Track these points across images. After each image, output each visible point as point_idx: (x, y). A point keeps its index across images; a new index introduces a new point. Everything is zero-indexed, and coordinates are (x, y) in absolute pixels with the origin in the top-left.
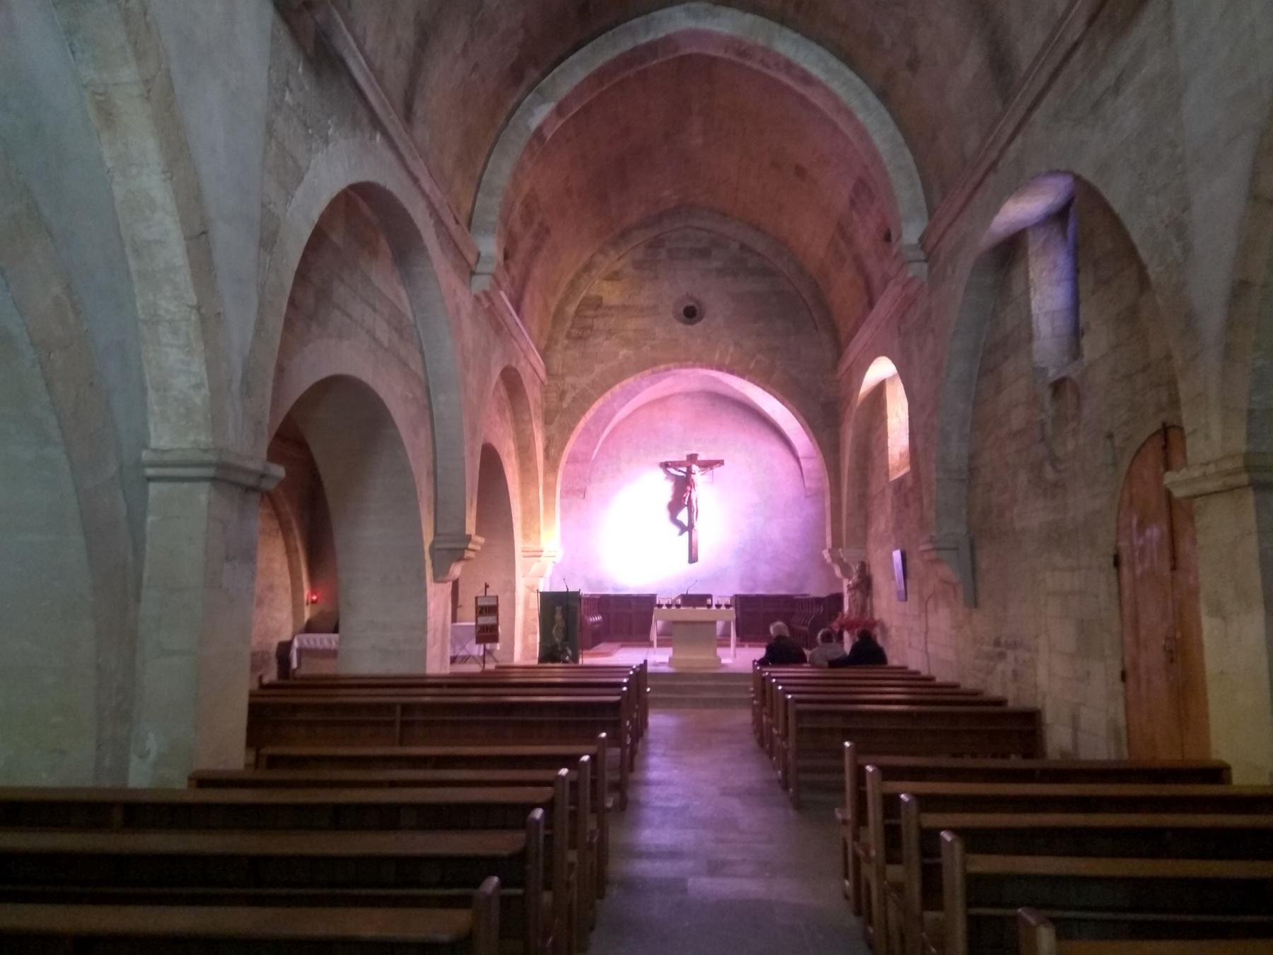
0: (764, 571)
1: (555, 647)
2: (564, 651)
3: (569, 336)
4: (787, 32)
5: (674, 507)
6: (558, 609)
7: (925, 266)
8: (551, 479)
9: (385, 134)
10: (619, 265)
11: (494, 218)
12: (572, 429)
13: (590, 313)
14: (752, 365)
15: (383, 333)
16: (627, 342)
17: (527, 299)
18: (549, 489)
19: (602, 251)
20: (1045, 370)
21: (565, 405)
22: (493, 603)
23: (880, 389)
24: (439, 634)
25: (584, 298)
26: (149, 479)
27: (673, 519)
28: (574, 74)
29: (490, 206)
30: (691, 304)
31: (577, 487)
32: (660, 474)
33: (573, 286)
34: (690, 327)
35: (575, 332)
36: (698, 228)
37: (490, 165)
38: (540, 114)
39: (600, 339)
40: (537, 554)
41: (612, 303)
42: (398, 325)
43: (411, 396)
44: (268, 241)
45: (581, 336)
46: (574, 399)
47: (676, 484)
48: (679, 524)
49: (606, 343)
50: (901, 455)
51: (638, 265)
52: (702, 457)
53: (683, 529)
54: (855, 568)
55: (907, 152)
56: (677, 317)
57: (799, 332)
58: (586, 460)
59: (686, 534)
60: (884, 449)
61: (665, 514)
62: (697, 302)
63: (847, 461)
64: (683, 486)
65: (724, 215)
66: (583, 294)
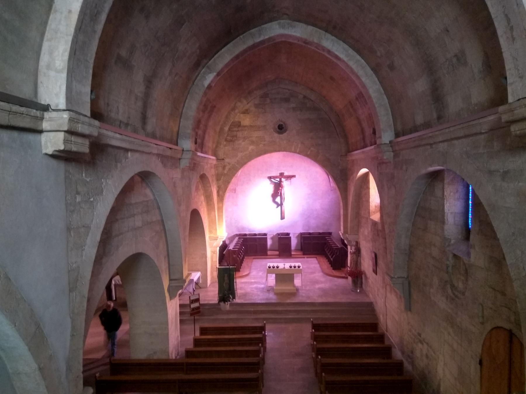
4: (329, 36)
6: (226, 275)
8: (221, 205)
9: (131, 150)
11: (189, 131)
14: (309, 153)
16: (252, 143)
20: (451, 240)
21: (225, 172)
22: (197, 297)
23: (366, 175)
24: (174, 320)
25: (233, 122)
28: (225, 57)
30: (282, 123)
32: (268, 182)
33: (227, 117)
34: (281, 135)
35: (229, 138)
37: (186, 105)
39: (240, 142)
41: (245, 125)
45: (232, 140)
46: (230, 169)
47: (275, 186)
49: (243, 143)
50: (376, 207)
51: (257, 106)
52: (286, 174)
54: (354, 243)
55: (385, 97)
59: (280, 207)
60: (368, 201)
61: (271, 199)
62: (284, 123)
63: (351, 198)
65: (296, 83)
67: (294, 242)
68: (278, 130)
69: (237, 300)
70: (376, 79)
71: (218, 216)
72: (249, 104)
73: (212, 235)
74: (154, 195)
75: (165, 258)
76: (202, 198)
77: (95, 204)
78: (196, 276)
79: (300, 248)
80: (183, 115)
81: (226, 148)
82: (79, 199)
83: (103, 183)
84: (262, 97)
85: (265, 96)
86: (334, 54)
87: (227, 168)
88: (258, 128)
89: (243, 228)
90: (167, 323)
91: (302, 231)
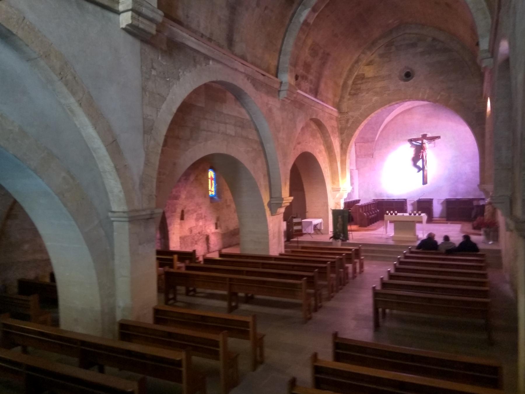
0: (461, 187)
3: (350, 94)
5: (415, 160)
6: (340, 216)
9: (213, 59)
12: (352, 136)
13: (360, 82)
14: (438, 98)
15: (231, 130)
16: (376, 94)
17: (322, 86)
18: (343, 162)
19: (363, 53)
21: (349, 125)
24: (276, 235)
25: (357, 76)
26: (113, 221)
27: (415, 165)
29: (286, 60)
30: (408, 70)
31: (369, 153)
32: (408, 145)
33: (351, 71)
34: (407, 83)
35: (353, 92)
36: (410, 34)
37: (285, 42)
38: (304, 14)
39: (364, 94)
40: (338, 190)
42: (241, 124)
44: (148, 129)
46: (353, 122)
49: (367, 95)
51: (381, 56)
52: (429, 135)
53: (420, 169)
57: (458, 76)
59: (421, 171)
61: (411, 163)
63: (488, 143)
66: (356, 74)
67: (437, 209)
68: (404, 78)
69: (350, 241)
73: (335, 186)
75: (264, 176)
76: (322, 148)
78: (316, 221)
80: (282, 52)
81: (350, 101)
82: (154, 73)
83: (180, 73)
85: (389, 45)
89: (381, 194)
90: (267, 233)
91: (448, 197)
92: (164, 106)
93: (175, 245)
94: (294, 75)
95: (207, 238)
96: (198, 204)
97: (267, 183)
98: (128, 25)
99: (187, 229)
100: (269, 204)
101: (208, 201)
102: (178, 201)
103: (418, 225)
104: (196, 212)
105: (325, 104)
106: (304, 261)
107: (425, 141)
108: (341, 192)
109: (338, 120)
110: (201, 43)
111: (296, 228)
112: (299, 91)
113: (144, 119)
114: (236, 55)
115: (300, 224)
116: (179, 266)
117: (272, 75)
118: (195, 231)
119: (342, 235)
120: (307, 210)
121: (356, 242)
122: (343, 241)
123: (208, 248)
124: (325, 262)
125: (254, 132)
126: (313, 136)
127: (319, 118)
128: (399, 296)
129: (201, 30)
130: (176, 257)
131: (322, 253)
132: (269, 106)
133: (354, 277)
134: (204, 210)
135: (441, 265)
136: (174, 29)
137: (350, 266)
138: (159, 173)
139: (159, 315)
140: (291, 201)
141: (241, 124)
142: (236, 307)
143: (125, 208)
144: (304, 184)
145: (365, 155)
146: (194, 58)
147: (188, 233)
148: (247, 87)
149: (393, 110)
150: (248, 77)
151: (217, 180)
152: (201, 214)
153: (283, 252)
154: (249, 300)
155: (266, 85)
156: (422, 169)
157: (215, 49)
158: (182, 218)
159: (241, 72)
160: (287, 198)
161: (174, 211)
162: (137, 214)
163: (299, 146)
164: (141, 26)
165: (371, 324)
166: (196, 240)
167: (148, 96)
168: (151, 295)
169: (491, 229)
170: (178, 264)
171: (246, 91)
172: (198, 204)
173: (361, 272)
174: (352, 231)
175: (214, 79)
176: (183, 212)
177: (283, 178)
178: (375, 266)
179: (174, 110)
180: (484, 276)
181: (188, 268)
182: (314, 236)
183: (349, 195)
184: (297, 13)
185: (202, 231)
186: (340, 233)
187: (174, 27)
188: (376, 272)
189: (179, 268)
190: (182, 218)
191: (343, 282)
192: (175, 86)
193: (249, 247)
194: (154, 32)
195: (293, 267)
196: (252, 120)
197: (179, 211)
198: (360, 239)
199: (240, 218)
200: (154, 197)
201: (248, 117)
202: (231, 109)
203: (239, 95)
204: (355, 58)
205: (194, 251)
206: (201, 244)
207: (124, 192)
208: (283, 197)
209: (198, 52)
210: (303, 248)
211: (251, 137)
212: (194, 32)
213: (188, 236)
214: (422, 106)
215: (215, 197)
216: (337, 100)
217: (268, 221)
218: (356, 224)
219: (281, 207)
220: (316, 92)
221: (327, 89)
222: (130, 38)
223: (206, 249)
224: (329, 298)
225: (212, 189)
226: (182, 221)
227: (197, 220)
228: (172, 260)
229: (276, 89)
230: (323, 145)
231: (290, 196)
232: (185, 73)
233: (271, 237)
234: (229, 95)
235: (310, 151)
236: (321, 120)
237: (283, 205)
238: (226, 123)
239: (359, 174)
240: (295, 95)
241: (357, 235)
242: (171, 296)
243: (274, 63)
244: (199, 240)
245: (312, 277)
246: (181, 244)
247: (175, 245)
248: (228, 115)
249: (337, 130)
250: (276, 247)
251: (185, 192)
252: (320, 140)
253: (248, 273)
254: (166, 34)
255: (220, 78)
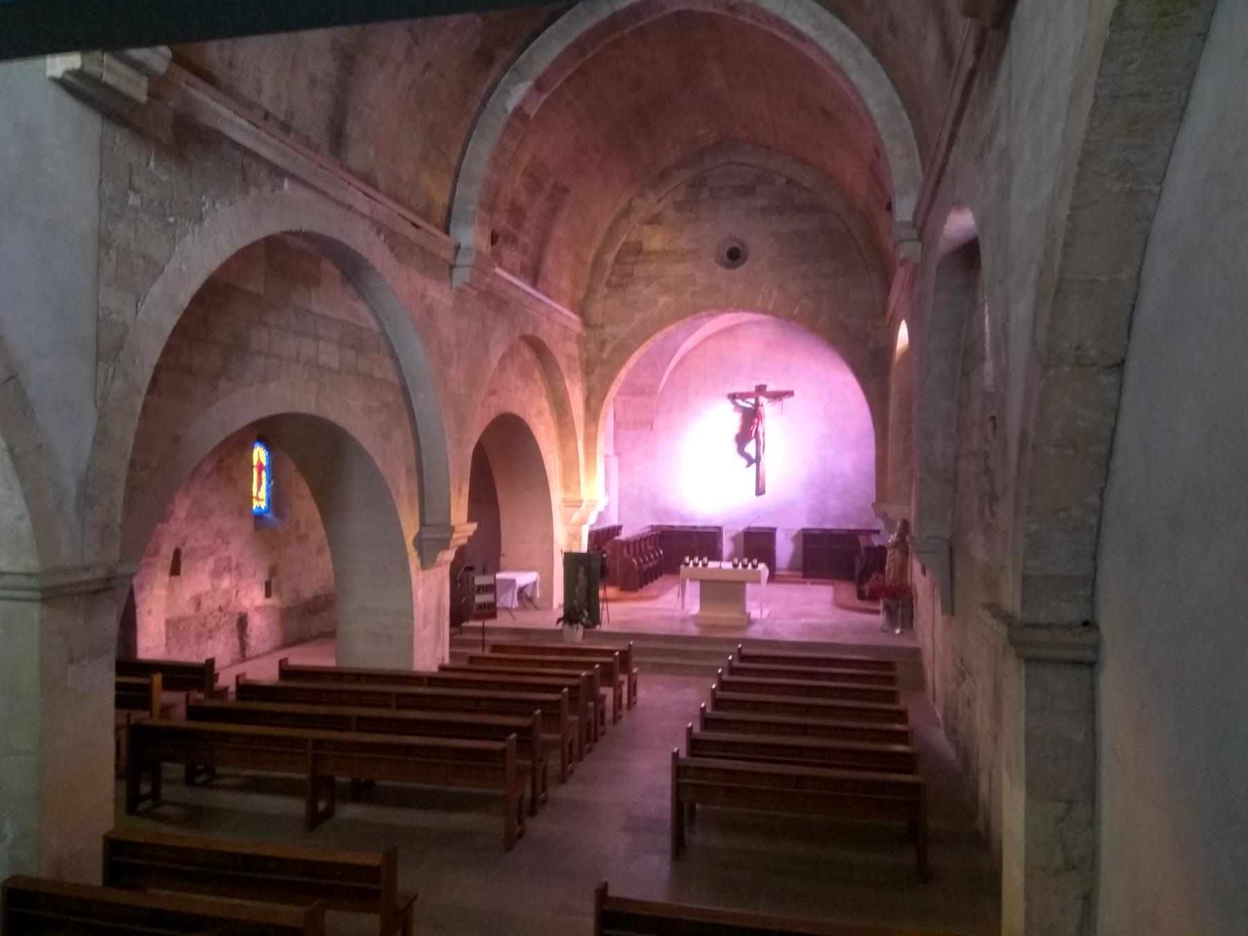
1: (573, 608)
2: (581, 612)
3: (609, 284)
6: (581, 569)
7: (919, 245)
9: (293, 177)
10: (659, 207)
11: (473, 207)
12: (612, 380)
13: (630, 259)
14: (796, 311)
15: (330, 356)
16: (667, 289)
17: (549, 261)
18: (591, 440)
19: (641, 194)
21: (605, 355)
24: (432, 617)
25: (625, 244)
27: (741, 450)
29: (470, 194)
30: (735, 245)
32: (728, 405)
33: (612, 231)
34: (732, 271)
35: (615, 280)
38: (517, 94)
40: (578, 504)
41: (651, 249)
42: (354, 340)
43: (378, 404)
44: (109, 349)
45: (621, 282)
46: (614, 350)
48: (747, 457)
49: (646, 291)
51: (679, 206)
52: (771, 387)
53: (750, 461)
55: (904, 114)
56: (720, 262)
57: (845, 272)
58: (652, 391)
59: (754, 466)
61: (733, 446)
62: (741, 243)
63: (893, 415)
64: (751, 418)
65: (769, 148)
66: (623, 239)
67: (784, 550)
68: (726, 259)
69: (604, 627)
70: (884, 75)
71: (587, 453)
72: (663, 203)
74: (380, 323)
75: (408, 471)
76: (544, 404)
77: (178, 232)
78: (525, 579)
79: (800, 564)
80: (461, 174)
82: (133, 200)
84: (691, 186)
85: (697, 184)
86: (793, 28)
87: (609, 347)
88: (681, 256)
89: (667, 513)
90: (410, 613)
91: (806, 526)
92: (156, 289)
93: (152, 643)
94: (488, 233)
95: (242, 623)
96: (219, 533)
97: (416, 489)
98: (69, 72)
99: (188, 598)
100: (418, 542)
101: (248, 525)
102: (166, 526)
103: (749, 588)
104: (212, 553)
105: (554, 305)
106: (504, 686)
107: (762, 400)
108: (583, 508)
109: (582, 342)
110: (263, 134)
111: (480, 599)
112: (498, 271)
113: (98, 320)
114: (349, 171)
115: (491, 588)
116: (173, 704)
117: (437, 226)
118: (209, 604)
119: (586, 613)
120: (503, 550)
121: (616, 630)
122: (586, 626)
123: (243, 646)
124: (557, 688)
125: (388, 363)
126: (525, 375)
127: (539, 335)
128: (730, 773)
129: (265, 101)
130: (157, 678)
131: (543, 663)
132: (428, 301)
133: (617, 718)
134: (234, 549)
135: (809, 691)
136: (195, 93)
137: (607, 692)
138: (132, 465)
139: (122, 858)
140: (471, 533)
141: (354, 340)
142: (329, 814)
143: (29, 562)
144: (498, 488)
145: (635, 424)
146: (244, 169)
147: (189, 610)
148: (376, 253)
149: (698, 328)
150: (379, 227)
151: (274, 468)
152: (229, 559)
153: (447, 661)
154: (362, 792)
155: (422, 249)
156: (755, 461)
157: (296, 150)
158: (175, 570)
159: (363, 216)
160: (463, 527)
161: (156, 552)
162: (70, 579)
163: (493, 400)
164: (108, 78)
165: (666, 841)
166: (209, 626)
167: (114, 258)
168: (97, 803)
169: (898, 603)
170: (162, 697)
171: (371, 262)
172: (219, 533)
173: (632, 703)
174: (606, 600)
175: (295, 228)
176: (177, 553)
177: (454, 476)
178: (660, 688)
179: (184, 299)
180: (901, 716)
181: (194, 712)
182: (517, 614)
183: (601, 516)
184: (499, 88)
185: (229, 603)
186: (581, 608)
187: (195, 87)
188: (668, 709)
189: (166, 709)
190: (175, 570)
191: (592, 732)
192: (189, 237)
193: (362, 650)
194: (143, 98)
195: (475, 705)
196: (383, 333)
197: (167, 551)
198: (624, 623)
199: (339, 574)
200: (118, 531)
201: (372, 323)
202: (330, 302)
203: (352, 269)
204: (623, 202)
205: (211, 662)
206: (223, 638)
207: (33, 520)
208: (453, 522)
209: (255, 156)
210: (496, 648)
211: (378, 374)
212: (245, 106)
213: (190, 618)
214: (757, 323)
215: (269, 515)
216: (580, 295)
217: (414, 583)
218: (613, 584)
219: (447, 547)
220: (534, 275)
221: (561, 267)
222: (71, 106)
223: (237, 649)
224: (563, 778)
225: (260, 497)
226: (174, 578)
227: (216, 574)
228: (147, 688)
229: (445, 261)
230: (547, 397)
231: (470, 520)
232: (218, 205)
233: (418, 621)
234: (328, 267)
235: (516, 410)
236: (545, 339)
237: (452, 544)
238: (317, 338)
239: (620, 466)
240: (488, 280)
241: (621, 612)
242: (145, 788)
243: (441, 198)
244: (218, 627)
245: (530, 729)
246: (168, 638)
247: (152, 643)
248: (324, 316)
249: (578, 364)
250: (430, 651)
251: (187, 503)
252: (540, 387)
253: (365, 724)
254: (172, 104)
255: (308, 224)
